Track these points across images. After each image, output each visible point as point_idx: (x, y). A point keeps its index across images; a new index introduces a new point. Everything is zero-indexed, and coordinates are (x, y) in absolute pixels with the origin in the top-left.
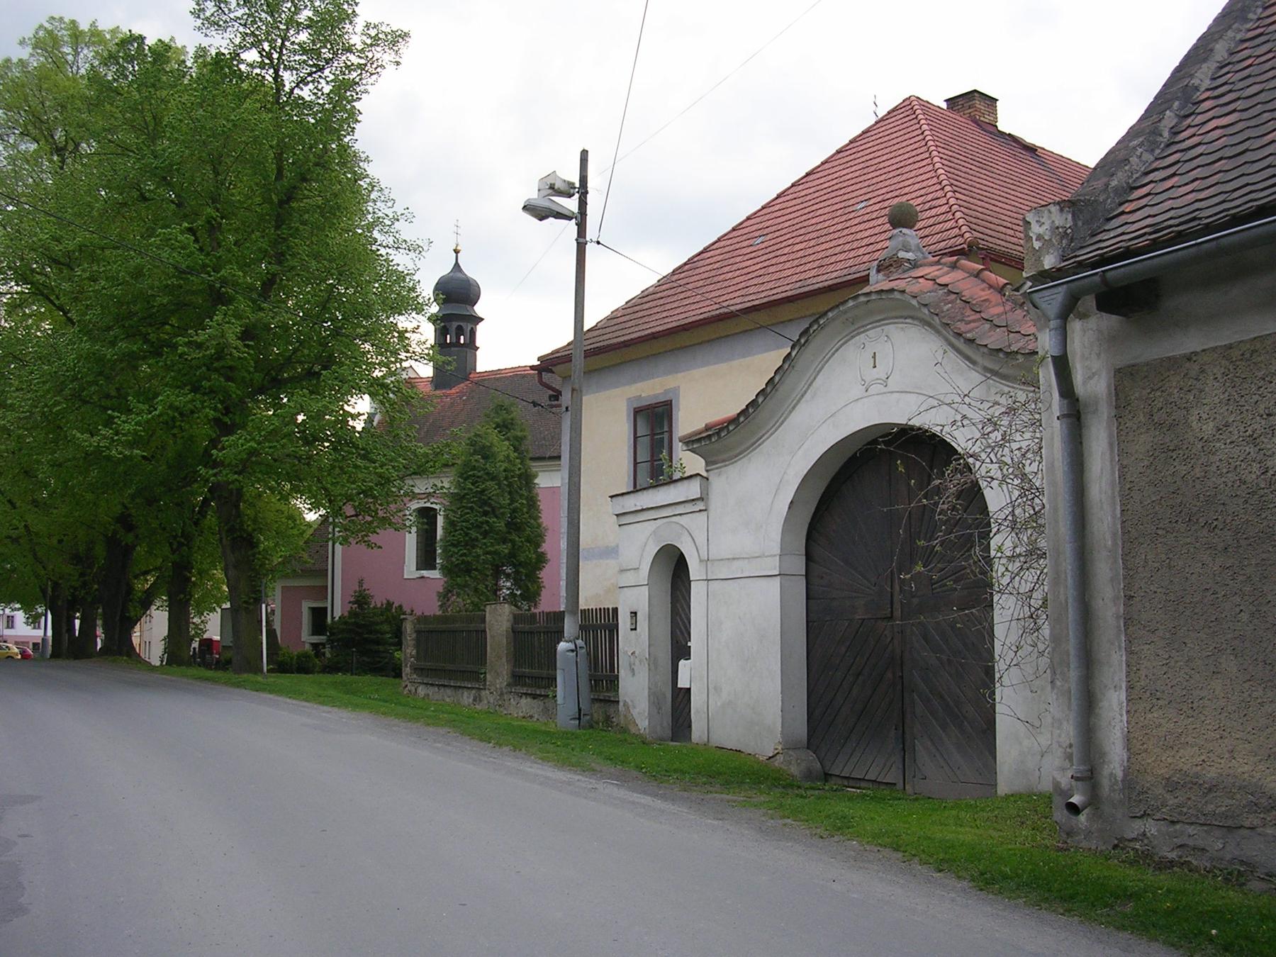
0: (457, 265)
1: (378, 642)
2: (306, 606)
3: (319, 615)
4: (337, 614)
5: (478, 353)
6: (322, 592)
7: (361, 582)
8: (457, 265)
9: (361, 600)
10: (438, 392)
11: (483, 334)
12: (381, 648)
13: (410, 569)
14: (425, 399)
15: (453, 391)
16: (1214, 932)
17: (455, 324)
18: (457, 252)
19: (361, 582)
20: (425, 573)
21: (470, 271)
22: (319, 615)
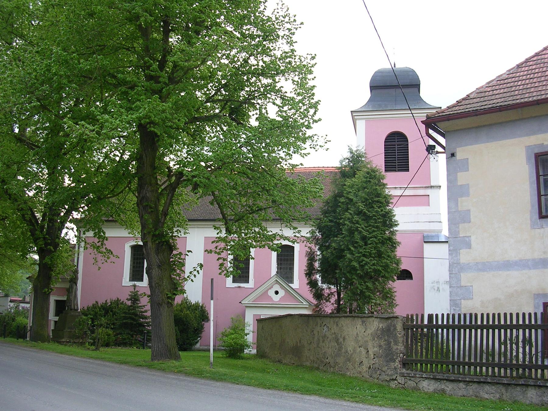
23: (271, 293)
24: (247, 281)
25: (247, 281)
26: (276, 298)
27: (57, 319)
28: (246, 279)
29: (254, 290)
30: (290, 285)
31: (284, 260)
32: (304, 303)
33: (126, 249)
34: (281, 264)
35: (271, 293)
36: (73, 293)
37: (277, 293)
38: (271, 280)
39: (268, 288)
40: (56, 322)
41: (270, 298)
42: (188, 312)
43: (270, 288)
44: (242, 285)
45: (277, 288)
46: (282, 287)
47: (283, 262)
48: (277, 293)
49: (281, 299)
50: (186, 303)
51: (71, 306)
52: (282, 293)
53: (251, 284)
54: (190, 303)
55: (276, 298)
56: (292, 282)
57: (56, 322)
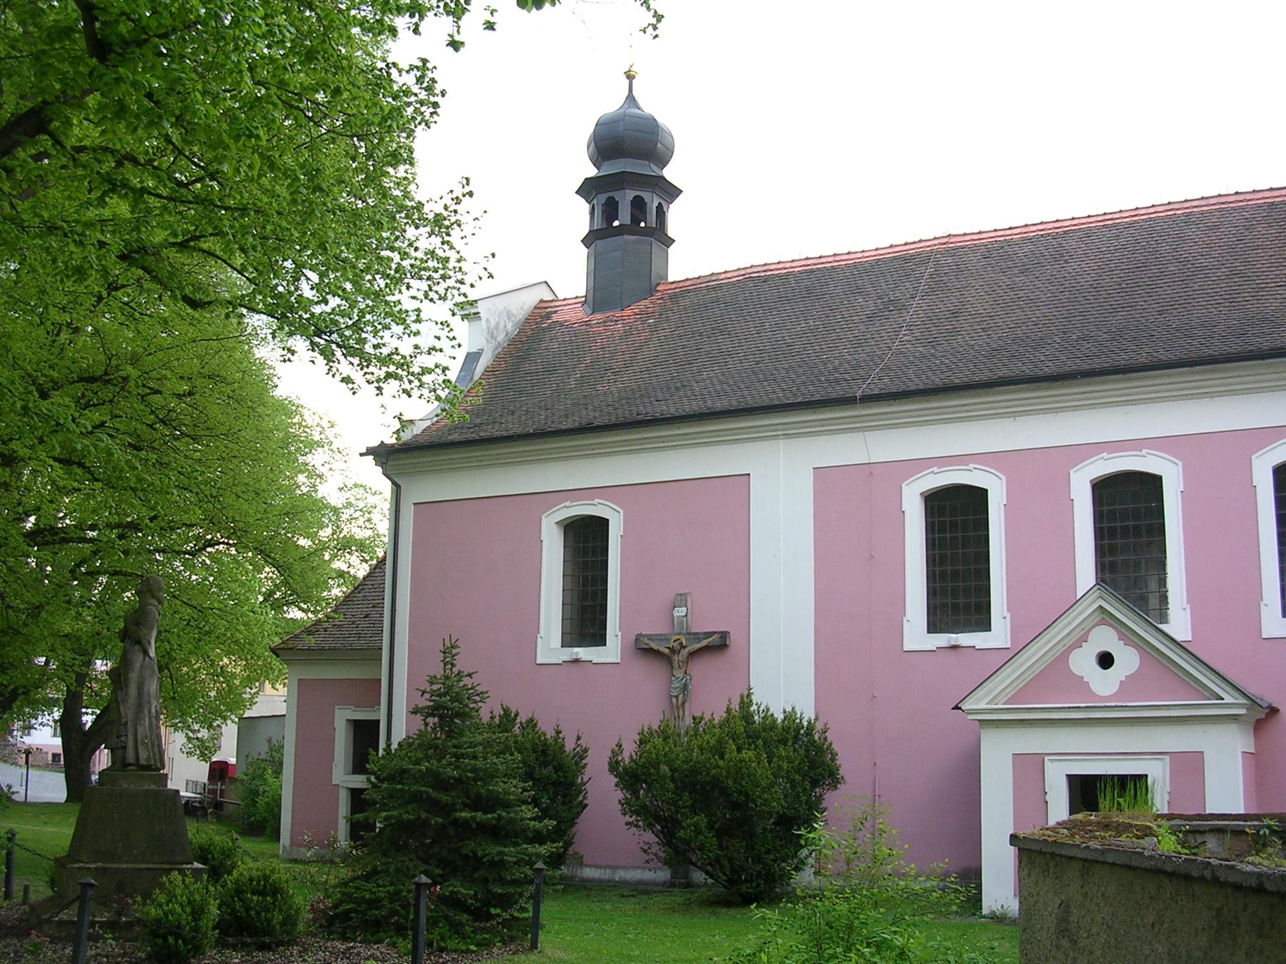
0: (631, 98)
1: (497, 833)
2: (342, 717)
3: (365, 733)
4: (399, 734)
5: (672, 250)
6: (369, 691)
7: (449, 653)
8: (631, 98)
9: (448, 707)
10: (598, 316)
11: (678, 218)
12: (510, 852)
13: (550, 643)
14: (579, 333)
15: (627, 312)
16: (49, 568)
17: (630, 194)
18: (630, 77)
19: (449, 653)
20: (582, 653)
21: (650, 105)
22: (365, 733)
23: (1083, 663)
24: (985, 625)
25: (985, 625)
26: (1105, 684)
27: (359, 781)
28: (980, 618)
29: (1011, 655)
30: (1160, 626)
31: (1125, 532)
32: (1228, 699)
33: (544, 536)
34: (1113, 550)
35: (1083, 663)
36: (133, 690)
37: (1106, 660)
38: (1078, 608)
39: (1069, 641)
40: (355, 793)
41: (1081, 685)
42: (748, 754)
43: (1078, 644)
44: (964, 639)
45: (1104, 639)
46: (1128, 636)
47: (1119, 542)
48: (1106, 660)
49: (1127, 686)
50: (747, 717)
51: (124, 748)
52: (1127, 660)
53: (999, 634)
54: (768, 716)
55: (1105, 684)
56: (1164, 618)
57: (355, 793)
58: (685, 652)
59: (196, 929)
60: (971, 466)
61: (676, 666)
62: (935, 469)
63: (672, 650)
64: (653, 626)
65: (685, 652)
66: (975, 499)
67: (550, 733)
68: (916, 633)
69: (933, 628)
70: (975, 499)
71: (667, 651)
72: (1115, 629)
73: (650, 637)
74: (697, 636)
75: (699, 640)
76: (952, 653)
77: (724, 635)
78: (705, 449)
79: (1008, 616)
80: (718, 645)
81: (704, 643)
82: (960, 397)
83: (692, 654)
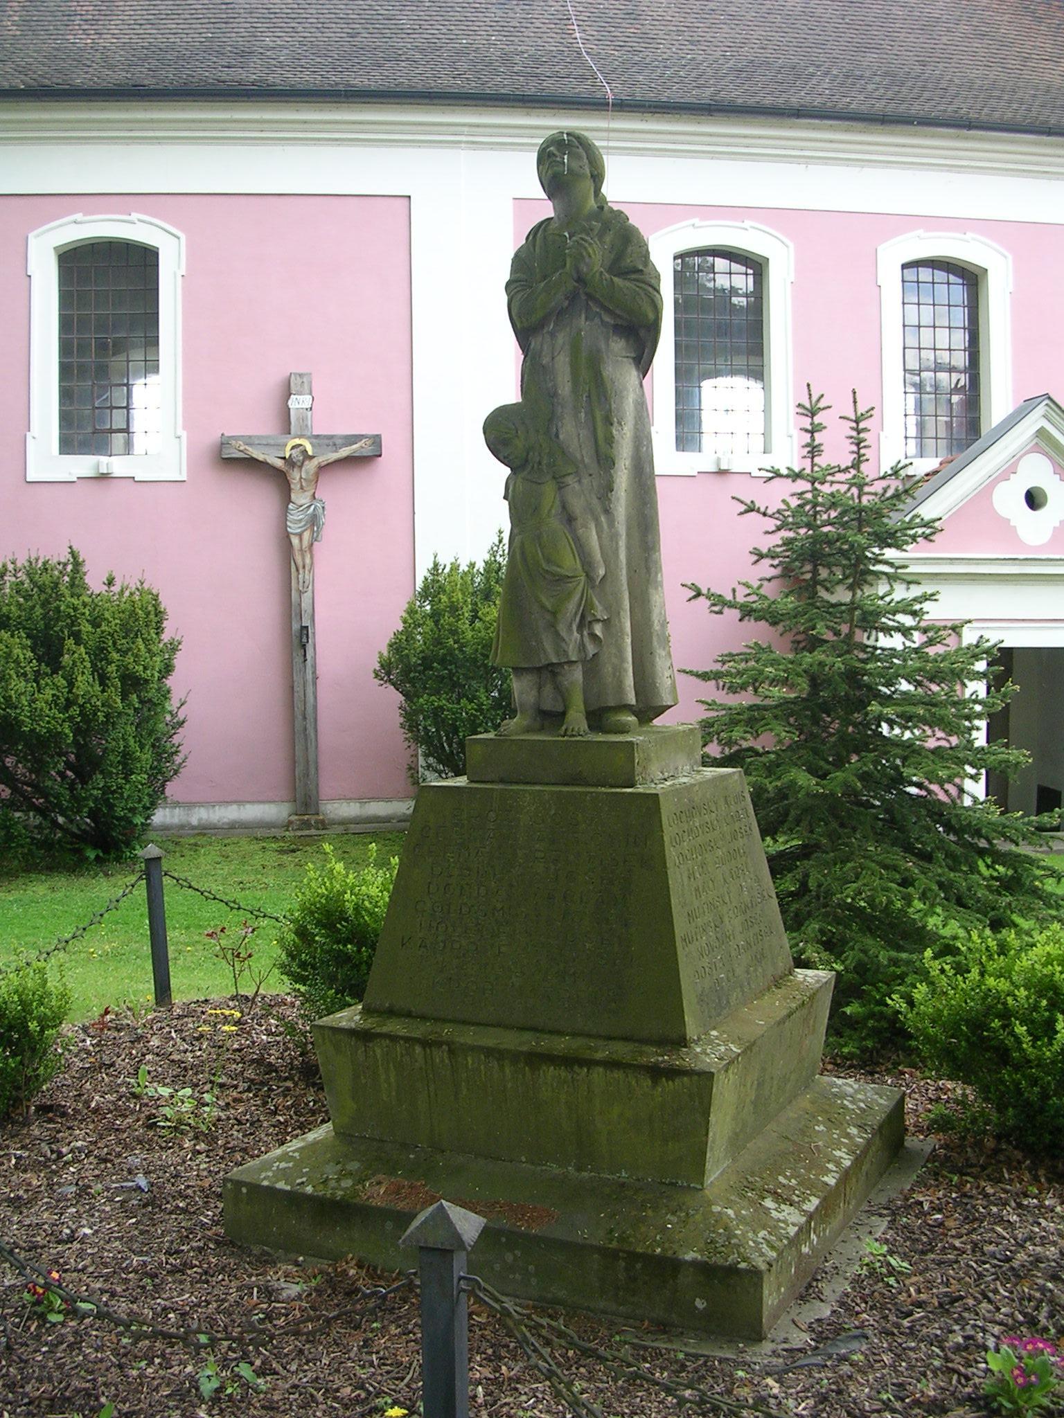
23: (1009, 500)
34: (83, 348)
37: (1034, 500)
41: (1005, 529)
58: (311, 466)
59: (140, 878)
60: (747, 224)
61: (295, 486)
62: (696, 221)
63: (290, 462)
64: (249, 424)
65: (311, 466)
66: (137, 263)
67: (766, 568)
68: (46, 457)
69: (68, 445)
70: (137, 263)
71: (279, 463)
72: (1050, 458)
73: (249, 440)
74: (330, 441)
75: (336, 447)
76: (718, 478)
77: (377, 440)
78: (854, 171)
79: (184, 435)
80: (360, 457)
81: (344, 452)
82: (747, 124)
83: (322, 468)
